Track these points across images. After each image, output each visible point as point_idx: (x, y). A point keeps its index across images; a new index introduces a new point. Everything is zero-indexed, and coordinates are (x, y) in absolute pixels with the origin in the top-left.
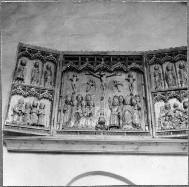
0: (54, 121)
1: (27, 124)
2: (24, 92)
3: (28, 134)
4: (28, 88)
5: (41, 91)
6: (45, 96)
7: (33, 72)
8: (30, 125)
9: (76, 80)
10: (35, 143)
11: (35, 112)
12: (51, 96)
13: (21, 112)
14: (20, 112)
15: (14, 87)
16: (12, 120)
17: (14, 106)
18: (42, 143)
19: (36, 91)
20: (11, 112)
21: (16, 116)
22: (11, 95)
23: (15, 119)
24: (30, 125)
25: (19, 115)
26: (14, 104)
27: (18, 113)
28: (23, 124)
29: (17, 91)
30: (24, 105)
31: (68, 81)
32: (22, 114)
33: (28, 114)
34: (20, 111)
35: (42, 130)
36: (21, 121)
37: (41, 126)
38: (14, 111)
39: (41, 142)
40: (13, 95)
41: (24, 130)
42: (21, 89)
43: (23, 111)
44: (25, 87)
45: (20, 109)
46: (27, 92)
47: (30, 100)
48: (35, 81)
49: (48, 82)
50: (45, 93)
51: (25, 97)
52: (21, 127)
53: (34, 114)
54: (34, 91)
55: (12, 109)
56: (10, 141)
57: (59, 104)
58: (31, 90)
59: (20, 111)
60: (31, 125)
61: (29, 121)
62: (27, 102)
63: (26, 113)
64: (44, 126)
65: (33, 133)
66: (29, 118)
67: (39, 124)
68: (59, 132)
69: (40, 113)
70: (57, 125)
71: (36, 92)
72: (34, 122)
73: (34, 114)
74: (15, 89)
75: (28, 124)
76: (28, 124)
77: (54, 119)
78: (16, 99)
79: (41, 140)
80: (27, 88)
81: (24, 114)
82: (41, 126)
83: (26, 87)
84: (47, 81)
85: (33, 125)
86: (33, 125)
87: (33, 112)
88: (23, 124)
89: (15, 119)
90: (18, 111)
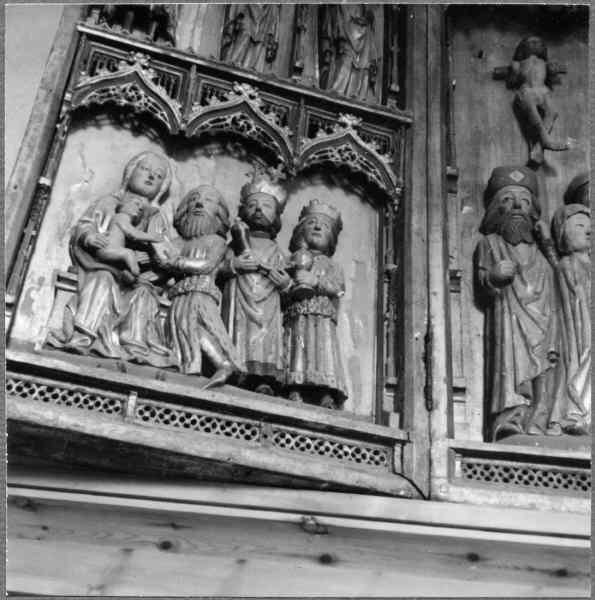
0: (427, 359)
1: (196, 366)
2: (175, 105)
3: (210, 462)
4: (207, 80)
5: (305, 114)
6: (335, 157)
7: (266, 273)
8: (221, 377)
9: (550, 80)
10: (270, 553)
11: (262, 271)
12: (385, 159)
13: (143, 257)
14: (134, 258)
15: (85, 54)
16: (57, 323)
17: (80, 209)
18: (325, 560)
19: (266, 109)
20: (50, 256)
21: (100, 292)
22: (62, 127)
23: (92, 316)
24: (221, 377)
25: (127, 286)
26: (84, 195)
27: (120, 264)
28: (157, 361)
29: (113, 89)
30: (168, 212)
31: (482, 83)
32: (152, 276)
33: (208, 282)
34: (131, 243)
35: (331, 430)
36: (136, 332)
37: (314, 393)
38: (84, 250)
39: (321, 545)
40: (83, 117)
41: (167, 418)
42: (148, 76)
43: (167, 248)
44: (188, 65)
45: (137, 233)
46: (198, 109)
47: (215, 179)
48: (253, 42)
49: (353, 68)
50: (338, 132)
51: (179, 145)
52: (143, 393)
53: (256, 285)
54: (256, 104)
55: (60, 237)
56: (27, 518)
57: (447, 120)
58: (233, 100)
59: (131, 243)
60: (234, 379)
61: (216, 341)
62: (190, 187)
63: (190, 273)
64: (338, 398)
65: (252, 455)
66: (212, 312)
67: (298, 378)
68: (476, 465)
69: (307, 279)
70: (445, 42)
71: (271, 119)
72: (258, 356)
73: (256, 285)
74: (104, 73)
75: (209, 367)
76: (209, 367)
77: (428, 338)
78: (100, 157)
79: (324, 531)
80: (195, 82)
81: (169, 277)
82: (314, 393)
83: (193, 74)
84: (339, 56)
85: (250, 381)
86: (250, 381)
87: (243, 272)
88: (157, 361)
89: (92, 316)
90: (115, 248)
